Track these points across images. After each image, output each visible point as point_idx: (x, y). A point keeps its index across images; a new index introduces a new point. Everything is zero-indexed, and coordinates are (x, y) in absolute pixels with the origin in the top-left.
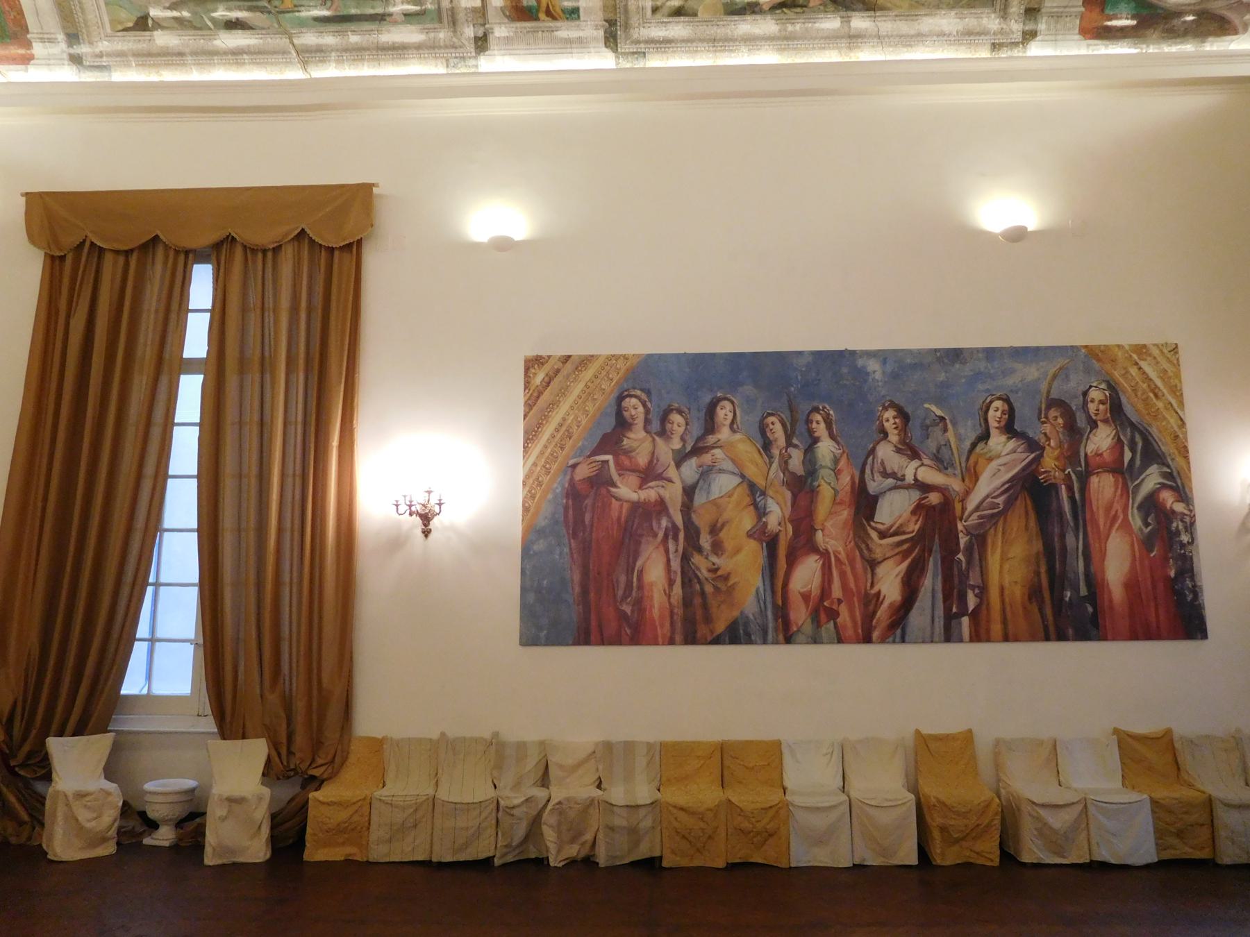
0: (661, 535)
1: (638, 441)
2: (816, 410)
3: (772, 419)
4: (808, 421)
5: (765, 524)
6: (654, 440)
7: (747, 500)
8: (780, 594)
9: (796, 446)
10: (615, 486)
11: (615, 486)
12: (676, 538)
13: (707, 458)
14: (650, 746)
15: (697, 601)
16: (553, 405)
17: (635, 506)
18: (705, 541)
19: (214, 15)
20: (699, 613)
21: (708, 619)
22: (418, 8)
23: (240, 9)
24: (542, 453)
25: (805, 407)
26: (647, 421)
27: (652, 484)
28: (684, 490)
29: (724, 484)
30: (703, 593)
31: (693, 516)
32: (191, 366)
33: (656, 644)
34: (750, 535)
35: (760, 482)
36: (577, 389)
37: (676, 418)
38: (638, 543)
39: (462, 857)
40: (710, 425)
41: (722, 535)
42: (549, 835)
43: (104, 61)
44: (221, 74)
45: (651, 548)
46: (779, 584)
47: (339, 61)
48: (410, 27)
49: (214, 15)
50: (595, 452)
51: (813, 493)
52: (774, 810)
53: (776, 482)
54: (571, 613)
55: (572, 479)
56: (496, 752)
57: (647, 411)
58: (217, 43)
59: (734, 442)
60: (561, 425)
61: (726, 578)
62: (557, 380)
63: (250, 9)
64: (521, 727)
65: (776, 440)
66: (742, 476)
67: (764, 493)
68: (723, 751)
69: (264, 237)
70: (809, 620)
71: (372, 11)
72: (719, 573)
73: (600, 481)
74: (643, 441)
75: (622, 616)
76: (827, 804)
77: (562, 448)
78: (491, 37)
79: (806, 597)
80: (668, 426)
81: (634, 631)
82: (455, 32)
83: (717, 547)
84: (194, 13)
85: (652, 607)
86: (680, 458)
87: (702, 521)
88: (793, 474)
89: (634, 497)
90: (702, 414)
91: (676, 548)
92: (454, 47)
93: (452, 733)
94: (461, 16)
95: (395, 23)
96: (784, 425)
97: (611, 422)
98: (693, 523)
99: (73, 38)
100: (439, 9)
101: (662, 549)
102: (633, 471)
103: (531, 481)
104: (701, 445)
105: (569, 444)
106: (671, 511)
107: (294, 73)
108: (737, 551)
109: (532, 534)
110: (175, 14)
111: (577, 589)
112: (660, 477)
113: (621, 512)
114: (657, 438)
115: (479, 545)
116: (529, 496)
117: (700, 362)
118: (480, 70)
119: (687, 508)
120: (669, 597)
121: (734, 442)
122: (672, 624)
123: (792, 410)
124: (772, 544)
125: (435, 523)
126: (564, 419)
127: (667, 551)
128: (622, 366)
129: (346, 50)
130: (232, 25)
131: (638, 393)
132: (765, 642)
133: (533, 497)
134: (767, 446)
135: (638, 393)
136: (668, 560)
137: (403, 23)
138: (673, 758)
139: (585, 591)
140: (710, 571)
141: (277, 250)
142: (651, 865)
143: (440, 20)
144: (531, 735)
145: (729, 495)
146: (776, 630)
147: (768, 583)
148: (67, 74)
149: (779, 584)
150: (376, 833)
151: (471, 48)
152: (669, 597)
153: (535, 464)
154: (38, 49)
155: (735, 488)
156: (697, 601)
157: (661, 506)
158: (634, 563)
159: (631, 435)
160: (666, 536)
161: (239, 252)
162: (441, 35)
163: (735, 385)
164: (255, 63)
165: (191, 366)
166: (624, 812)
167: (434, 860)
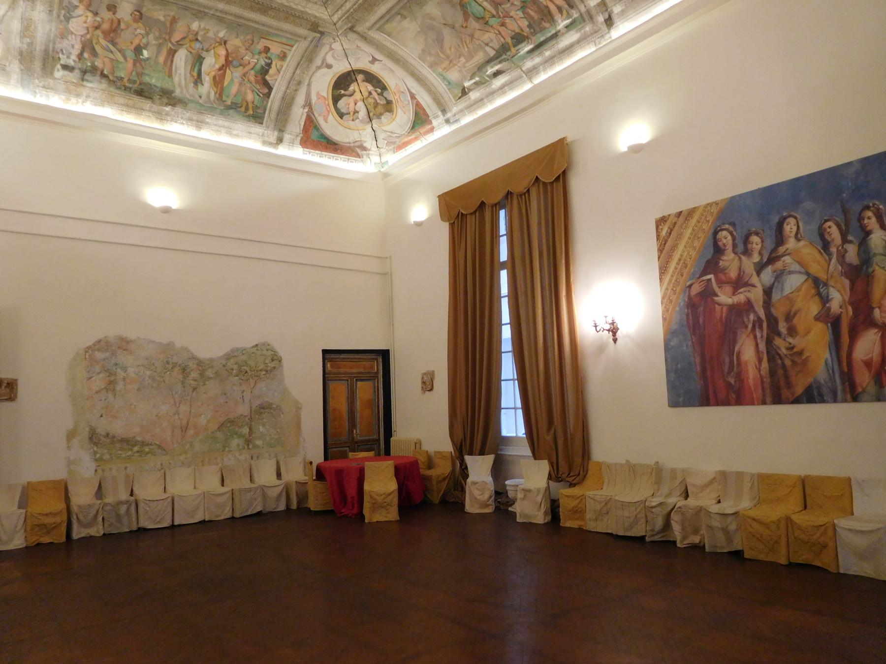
0: (750, 326)
1: (730, 261)
2: (867, 208)
3: (829, 224)
4: (860, 219)
5: (829, 309)
6: (740, 258)
7: (813, 291)
8: (845, 364)
9: (851, 242)
10: (716, 295)
11: (716, 295)
12: (761, 327)
13: (779, 265)
14: (752, 475)
15: (780, 372)
16: (674, 247)
17: (731, 307)
18: (783, 327)
19: (488, 73)
20: (782, 383)
21: (789, 385)
22: (570, 20)
23: (495, 65)
24: (670, 281)
25: (856, 207)
26: (735, 246)
27: (742, 290)
28: (764, 291)
29: (794, 282)
30: (784, 366)
31: (773, 310)
32: (503, 265)
33: (753, 404)
34: (817, 319)
35: (823, 276)
36: (688, 233)
37: (755, 239)
38: (735, 333)
39: (628, 534)
40: (780, 239)
41: (795, 321)
42: (676, 527)
43: (457, 117)
44: (500, 101)
45: (744, 336)
46: (844, 354)
47: (545, 70)
48: (571, 33)
49: (488, 73)
50: (705, 272)
51: (869, 278)
52: (823, 528)
53: (835, 274)
54: (697, 385)
55: (689, 296)
56: (657, 473)
57: (734, 239)
58: (493, 86)
59: (799, 248)
60: (680, 260)
61: (800, 353)
62: (677, 227)
63: (500, 62)
64: (673, 460)
65: (833, 240)
66: (808, 274)
67: (826, 284)
68: (804, 483)
69: (519, 187)
70: (873, 383)
71: (550, 34)
72: (795, 350)
73: (707, 294)
74: (733, 259)
75: (729, 385)
76: (870, 529)
77: (682, 276)
78: (613, 15)
79: (868, 364)
80: (750, 246)
81: (736, 396)
82: (593, 23)
83: (792, 331)
84: (480, 77)
85: (748, 378)
86: (760, 268)
87: (779, 312)
88: (850, 265)
89: (729, 301)
90: (773, 232)
91: (762, 334)
92: (596, 32)
93: (633, 461)
94: (593, 12)
95: (563, 34)
96: (839, 226)
97: (711, 251)
98: (772, 315)
99: (444, 111)
100: (581, 15)
101: (752, 336)
102: (728, 283)
103: (666, 300)
104: (774, 255)
105: (686, 271)
106: (756, 309)
107: (527, 86)
108: (808, 332)
109: (670, 335)
110: (473, 81)
111: (699, 369)
112: (747, 284)
113: (722, 313)
114: (743, 258)
115: (642, 344)
116: (666, 311)
117: (769, 194)
118: (613, 38)
119: (767, 304)
120: (760, 370)
121: (799, 248)
122: (763, 389)
123: (845, 212)
124: (835, 323)
125: (619, 334)
126: (681, 255)
127: (755, 337)
128: (715, 210)
129: (546, 62)
130: (496, 74)
131: (727, 226)
132: (835, 401)
133: (668, 311)
134: (826, 246)
135: (727, 226)
136: (757, 345)
137: (567, 32)
138: (767, 485)
139: (704, 370)
140: (788, 349)
141: (528, 190)
142: (738, 554)
143: (584, 21)
144: (680, 465)
145: (798, 289)
146: (844, 390)
147: (834, 354)
148: (446, 130)
149: (844, 354)
150: (589, 515)
151: (604, 27)
152: (760, 370)
153: (667, 289)
154: (435, 123)
155: (802, 284)
156: (780, 372)
157: (749, 305)
158: (734, 348)
159: (725, 258)
160: (754, 326)
161: (515, 198)
162: (587, 29)
163: (796, 203)
164: (511, 89)
165: (503, 265)
166: (718, 518)
167: (238, 515)
